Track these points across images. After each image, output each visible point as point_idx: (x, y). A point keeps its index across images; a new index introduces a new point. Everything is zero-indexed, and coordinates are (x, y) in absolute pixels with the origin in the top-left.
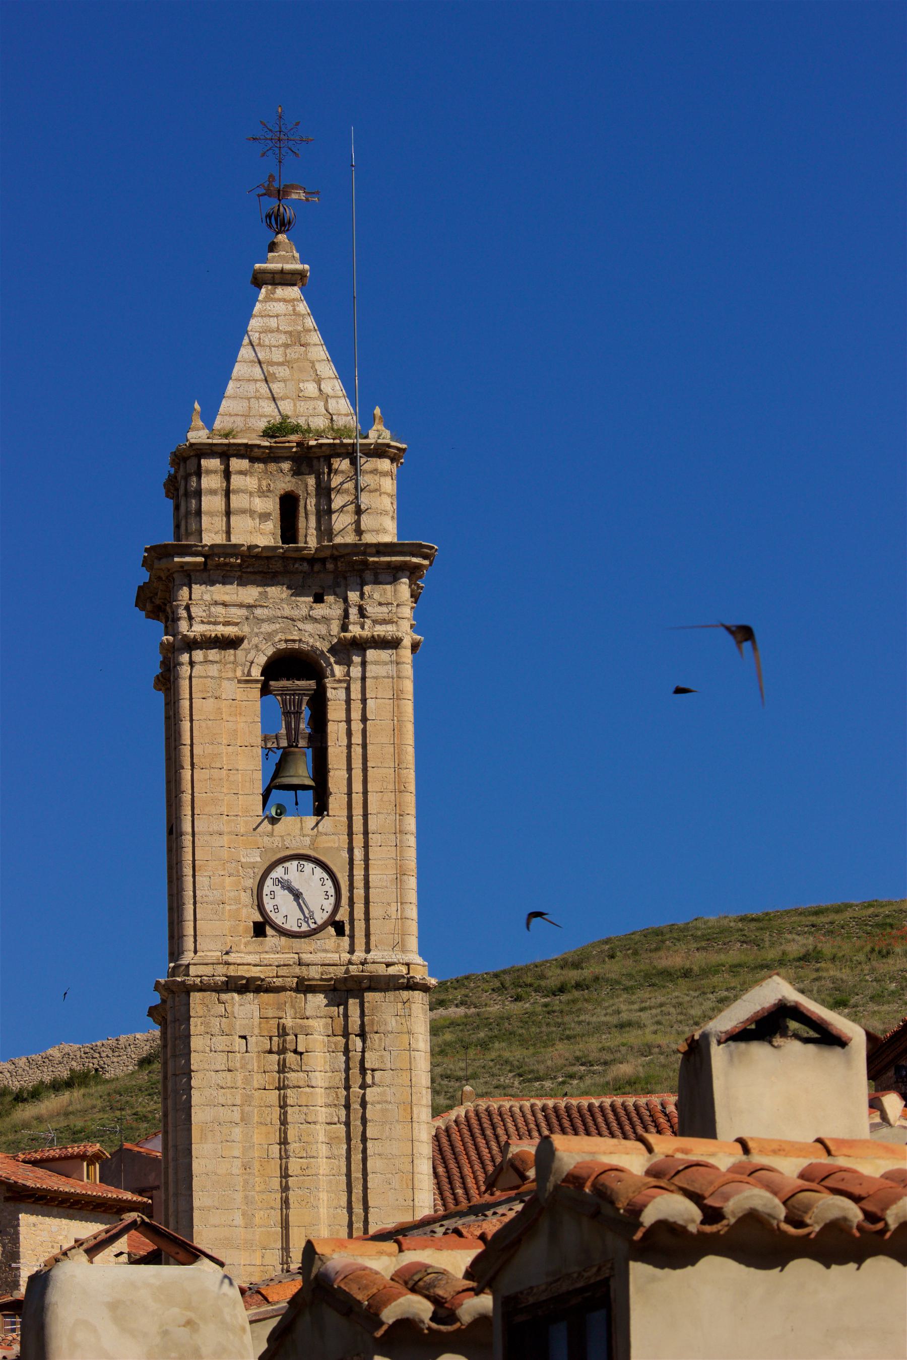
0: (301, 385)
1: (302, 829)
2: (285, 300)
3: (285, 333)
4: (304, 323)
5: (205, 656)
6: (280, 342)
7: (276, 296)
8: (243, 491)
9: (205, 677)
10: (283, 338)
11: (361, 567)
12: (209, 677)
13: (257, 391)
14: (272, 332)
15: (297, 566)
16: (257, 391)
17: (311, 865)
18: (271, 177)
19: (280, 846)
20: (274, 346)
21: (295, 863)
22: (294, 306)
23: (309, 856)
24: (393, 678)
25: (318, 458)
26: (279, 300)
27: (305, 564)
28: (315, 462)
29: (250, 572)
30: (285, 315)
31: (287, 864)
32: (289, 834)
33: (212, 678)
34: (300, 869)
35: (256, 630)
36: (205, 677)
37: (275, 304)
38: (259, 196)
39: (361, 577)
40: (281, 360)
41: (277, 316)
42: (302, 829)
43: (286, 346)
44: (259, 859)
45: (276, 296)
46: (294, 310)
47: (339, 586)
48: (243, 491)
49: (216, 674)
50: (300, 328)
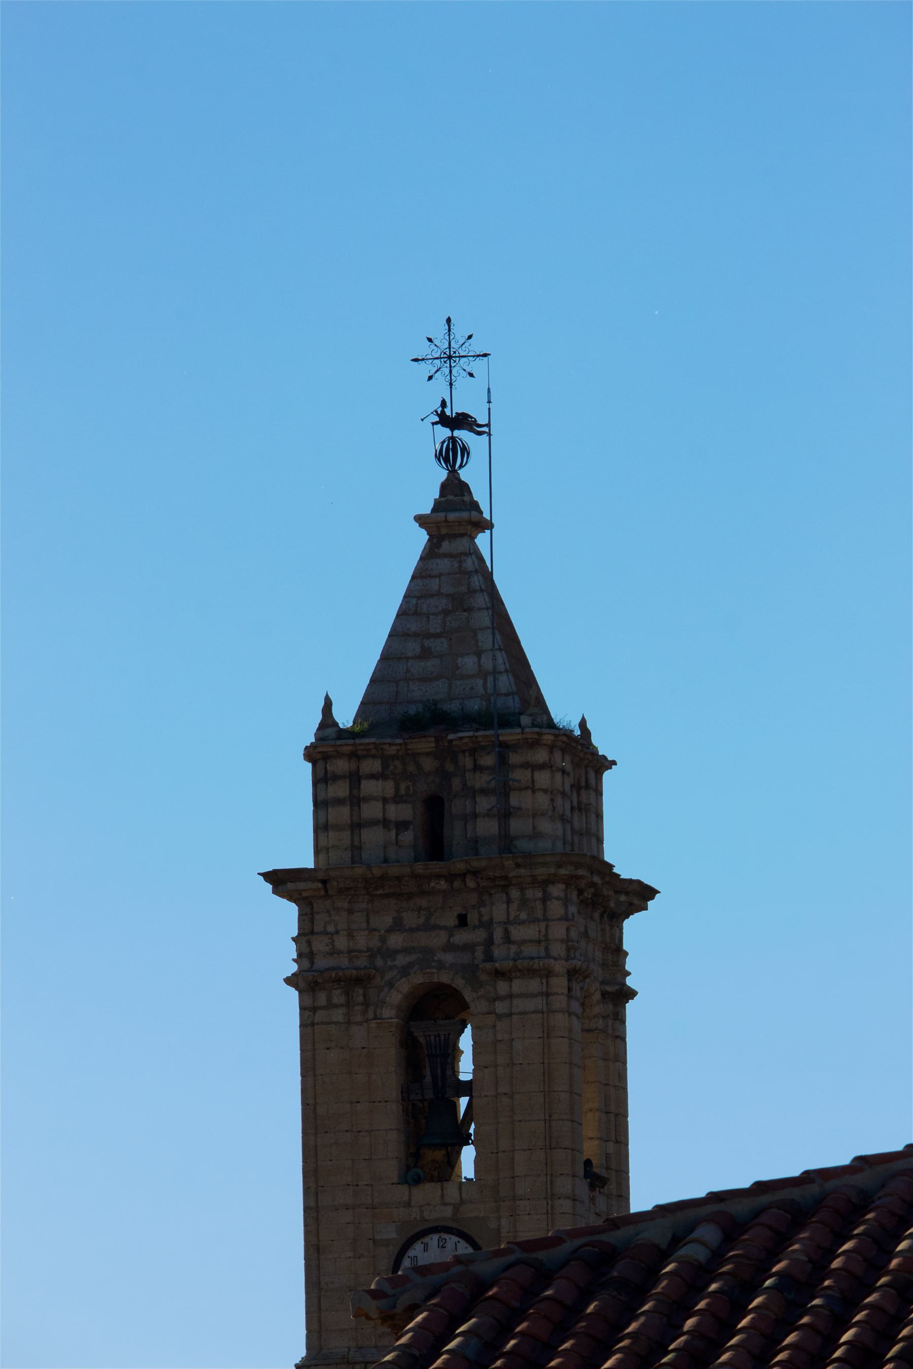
0: (459, 660)
1: (442, 1196)
2: (450, 556)
3: (448, 596)
4: (469, 583)
5: (329, 999)
6: (440, 608)
7: (442, 551)
8: (375, 799)
9: (329, 1023)
10: (443, 603)
11: (503, 883)
12: (333, 1022)
13: (408, 671)
14: (432, 596)
15: (432, 884)
16: (408, 671)
17: (455, 1239)
18: (443, 404)
19: (418, 1217)
20: (433, 614)
21: (435, 1237)
22: (460, 562)
23: (451, 1228)
24: (543, 1013)
25: (463, 752)
26: (445, 556)
27: (443, 882)
28: (461, 756)
29: (381, 895)
30: (449, 574)
31: (426, 1240)
32: (428, 1204)
33: (336, 1023)
34: (441, 1244)
35: (390, 963)
36: (329, 1023)
37: (438, 561)
38: (433, 424)
39: (507, 893)
40: (438, 631)
41: (440, 576)
42: (442, 1196)
43: (446, 612)
44: (394, 1235)
45: (442, 551)
46: (460, 566)
47: (485, 906)
48: (375, 799)
49: (340, 1018)
50: (464, 589)
